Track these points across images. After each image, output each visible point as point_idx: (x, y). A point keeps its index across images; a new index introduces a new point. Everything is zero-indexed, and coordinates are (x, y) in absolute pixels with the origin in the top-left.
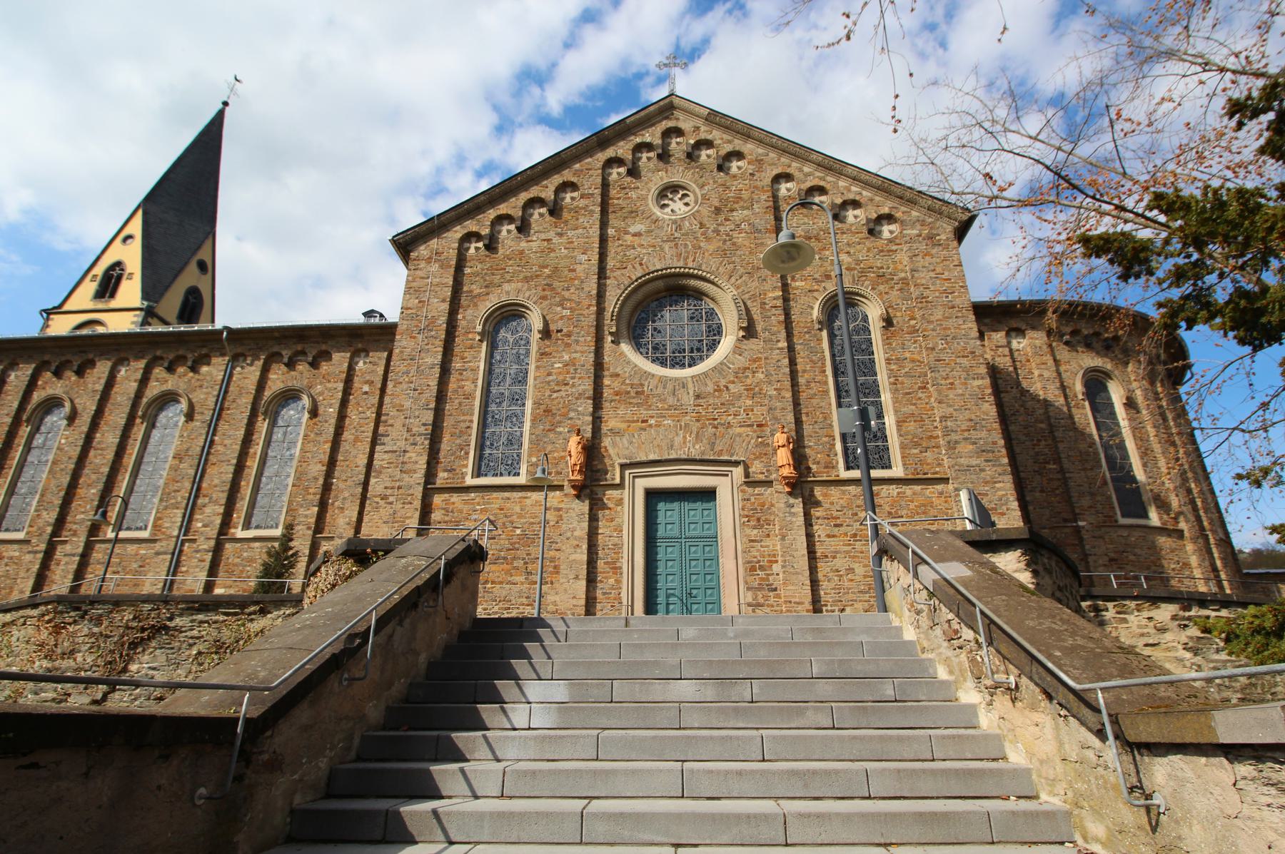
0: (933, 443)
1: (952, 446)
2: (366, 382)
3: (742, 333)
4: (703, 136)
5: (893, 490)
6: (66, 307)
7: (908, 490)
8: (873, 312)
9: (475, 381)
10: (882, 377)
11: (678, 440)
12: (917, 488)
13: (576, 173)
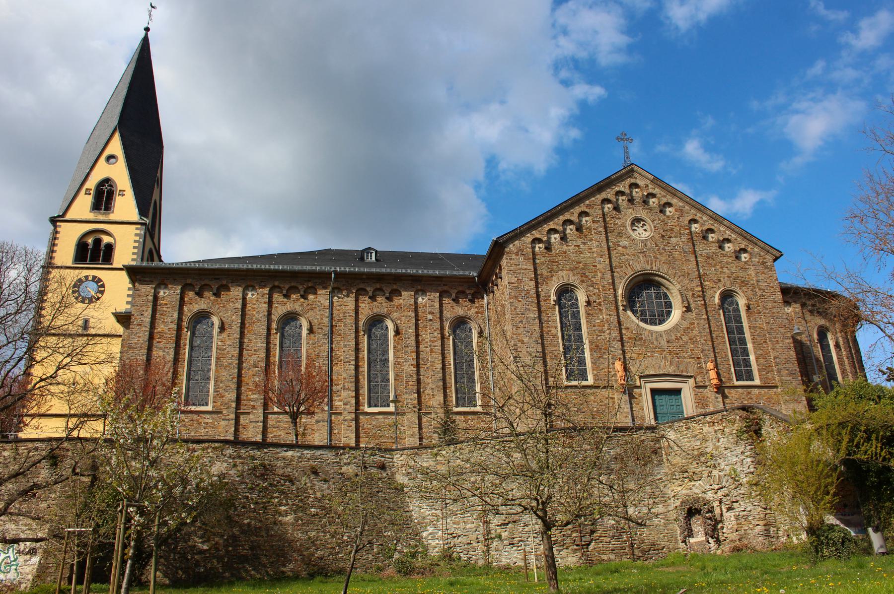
1: (779, 371)
3: (684, 309)
4: (651, 191)
5: (756, 391)
6: (69, 216)
7: (763, 391)
8: (742, 302)
9: (556, 327)
10: (747, 335)
11: (662, 364)
12: (766, 390)
13: (588, 206)
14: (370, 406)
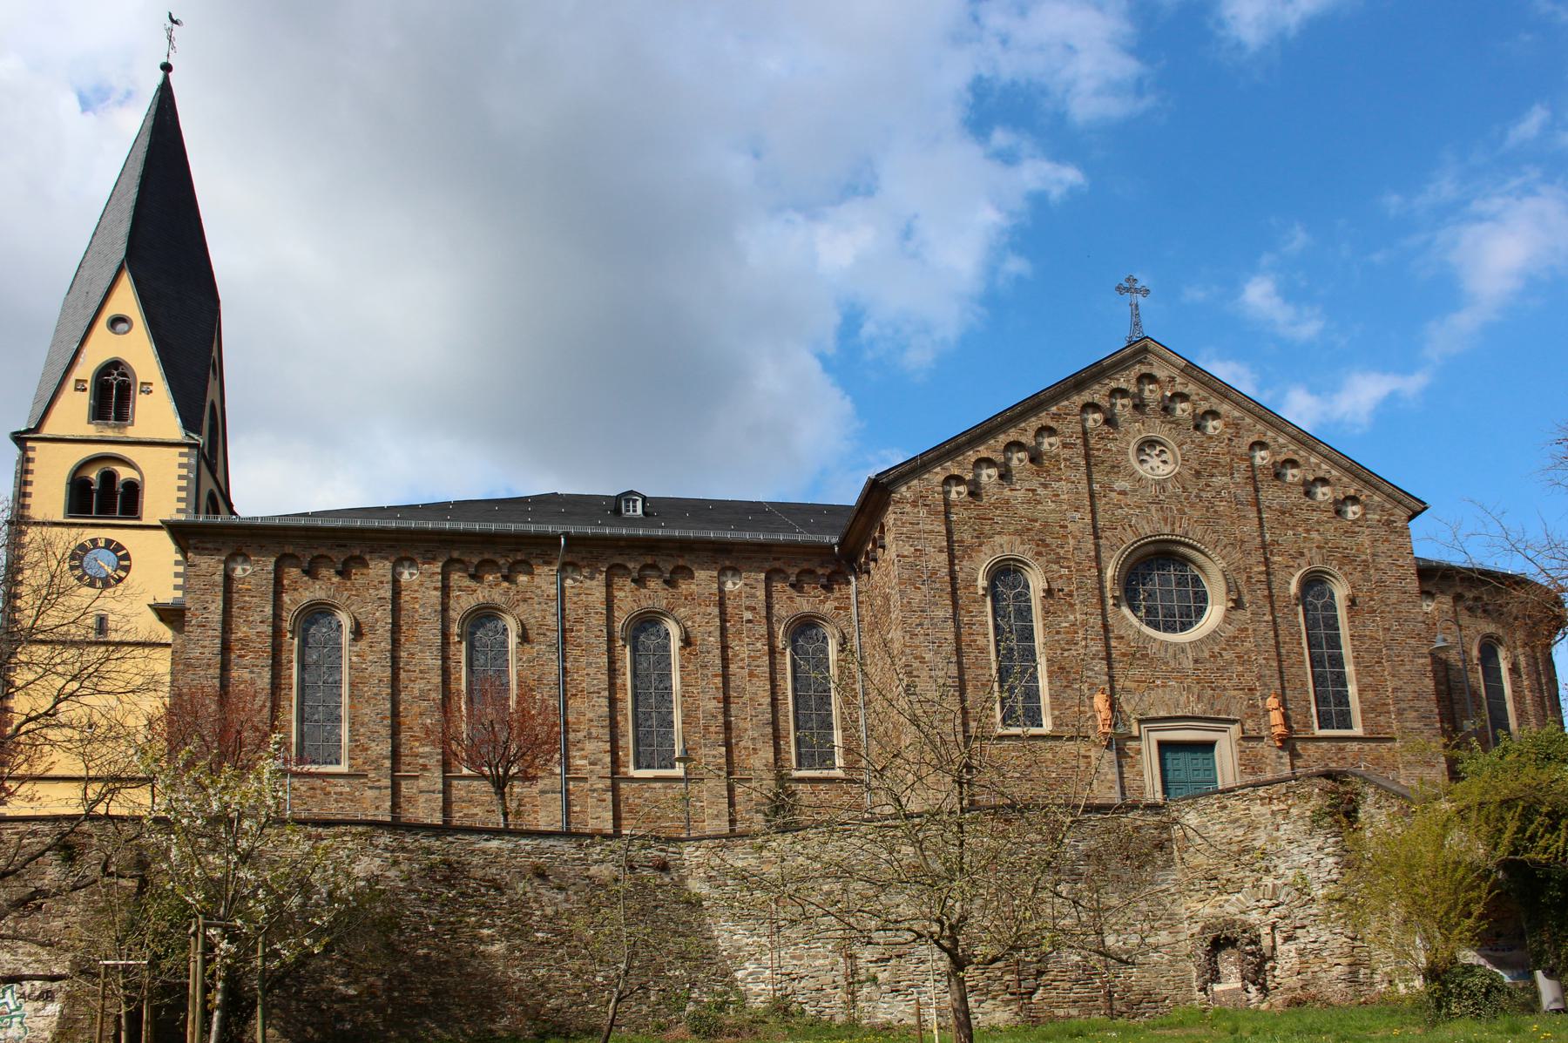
0: (1385, 709)
1: (1400, 712)
2: (748, 608)
3: (1231, 604)
4: (1179, 388)
5: (1355, 746)
7: (1366, 746)
9: (986, 635)
10: (1347, 651)
14: (638, 766)
